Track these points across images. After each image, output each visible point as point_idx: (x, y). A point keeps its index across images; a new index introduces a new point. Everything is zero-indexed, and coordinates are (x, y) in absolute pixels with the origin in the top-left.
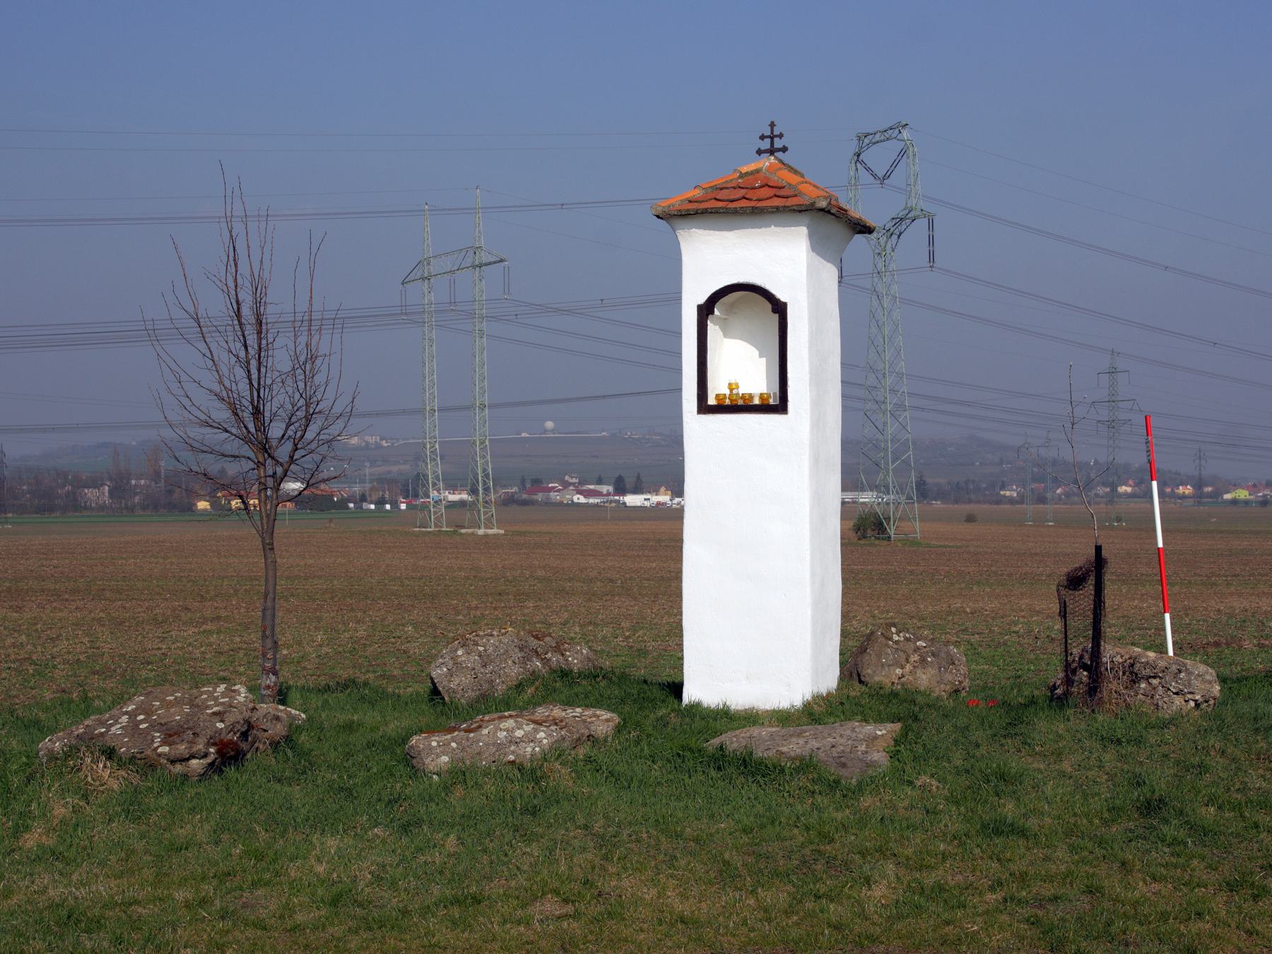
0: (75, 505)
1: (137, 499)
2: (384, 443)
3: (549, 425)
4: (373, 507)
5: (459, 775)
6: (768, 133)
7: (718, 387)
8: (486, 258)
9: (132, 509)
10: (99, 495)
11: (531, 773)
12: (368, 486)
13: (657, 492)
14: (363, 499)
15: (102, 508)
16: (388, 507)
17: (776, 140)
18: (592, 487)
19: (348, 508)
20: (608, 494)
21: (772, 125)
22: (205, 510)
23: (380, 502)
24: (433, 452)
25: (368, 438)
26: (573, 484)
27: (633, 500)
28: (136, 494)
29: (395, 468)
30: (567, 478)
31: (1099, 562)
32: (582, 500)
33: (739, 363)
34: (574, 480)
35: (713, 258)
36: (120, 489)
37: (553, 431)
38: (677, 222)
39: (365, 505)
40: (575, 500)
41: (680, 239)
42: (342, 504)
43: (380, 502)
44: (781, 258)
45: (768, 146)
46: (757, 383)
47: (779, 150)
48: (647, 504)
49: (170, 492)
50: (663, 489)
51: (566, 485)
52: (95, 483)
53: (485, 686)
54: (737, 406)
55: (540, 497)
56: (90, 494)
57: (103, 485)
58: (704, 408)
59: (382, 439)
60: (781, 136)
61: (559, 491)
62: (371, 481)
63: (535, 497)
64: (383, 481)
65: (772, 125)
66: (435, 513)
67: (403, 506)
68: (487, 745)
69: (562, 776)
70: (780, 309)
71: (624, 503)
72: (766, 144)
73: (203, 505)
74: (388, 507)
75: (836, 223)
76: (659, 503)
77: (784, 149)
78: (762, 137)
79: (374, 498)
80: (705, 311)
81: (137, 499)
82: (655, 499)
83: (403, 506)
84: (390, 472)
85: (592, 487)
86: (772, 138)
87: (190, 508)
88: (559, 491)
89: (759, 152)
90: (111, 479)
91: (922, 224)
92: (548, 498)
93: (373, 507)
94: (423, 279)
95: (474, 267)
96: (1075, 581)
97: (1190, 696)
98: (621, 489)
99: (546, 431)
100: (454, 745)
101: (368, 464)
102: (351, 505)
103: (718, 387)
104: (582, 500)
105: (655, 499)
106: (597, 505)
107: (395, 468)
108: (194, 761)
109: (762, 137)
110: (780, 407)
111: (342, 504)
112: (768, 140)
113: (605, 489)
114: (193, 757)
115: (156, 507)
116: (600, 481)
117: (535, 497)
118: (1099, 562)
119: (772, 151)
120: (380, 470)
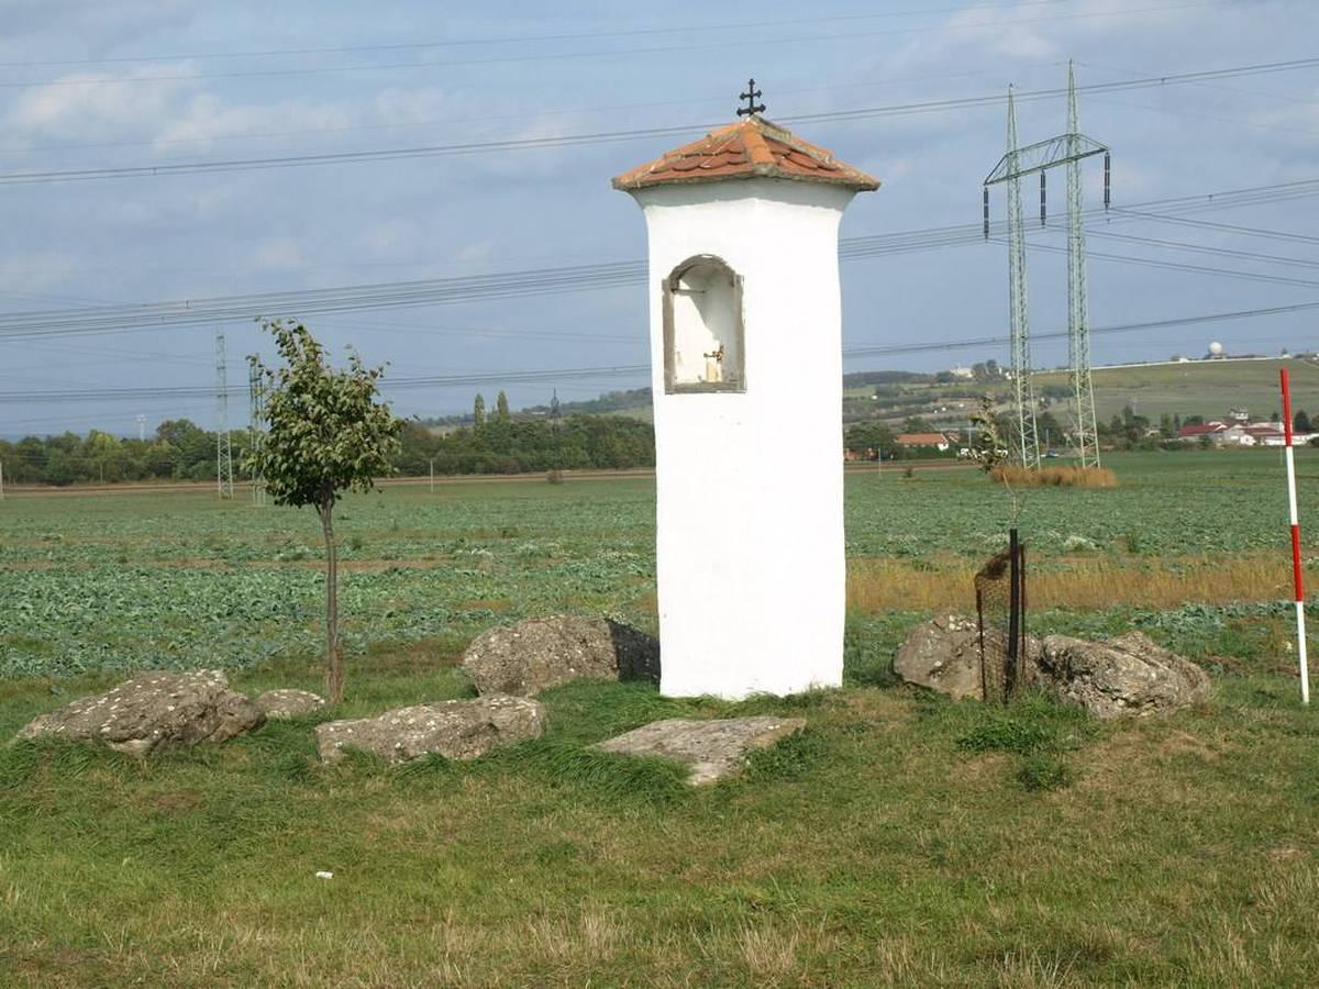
6: (747, 92)
17: (755, 98)
18: (1265, 425)
21: (752, 83)
26: (1241, 422)
31: (1016, 550)
37: (1221, 356)
38: (645, 197)
41: (648, 219)
45: (748, 106)
47: (757, 109)
51: (1231, 422)
53: (513, 674)
58: (673, 389)
60: (759, 94)
65: (752, 83)
66: (1029, 463)
68: (379, 731)
72: (745, 104)
77: (762, 108)
78: (743, 97)
86: (751, 96)
89: (740, 113)
97: (1117, 694)
100: (350, 731)
108: (136, 742)
109: (743, 97)
112: (748, 99)
114: (134, 736)
118: (1016, 550)
119: (751, 111)
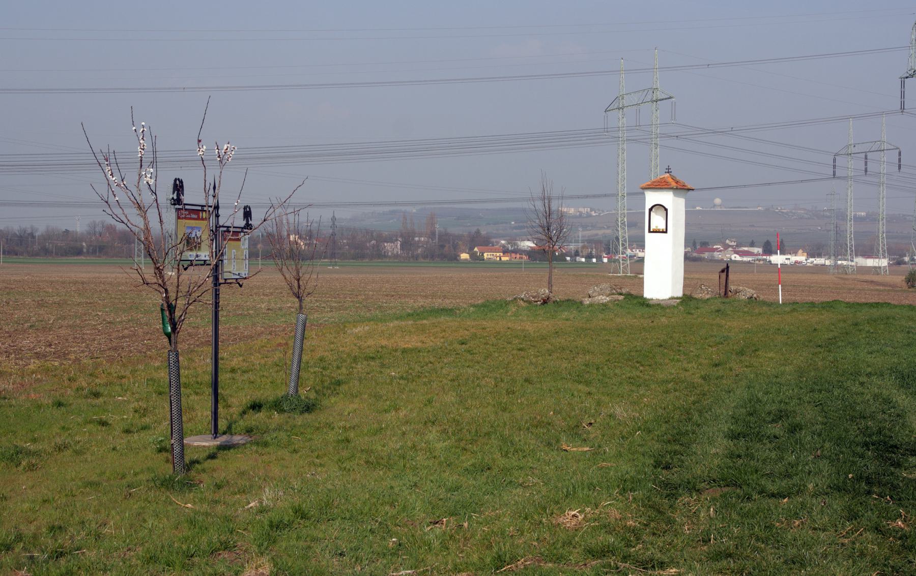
0: (379, 254)
1: (420, 251)
2: (593, 214)
3: (718, 201)
4: (583, 260)
5: (591, 305)
7: (653, 227)
8: (660, 95)
9: (416, 258)
10: (393, 248)
11: (605, 305)
12: (580, 245)
13: (796, 253)
14: (577, 254)
15: (396, 256)
16: (594, 260)
18: (746, 249)
19: (566, 260)
20: (758, 254)
22: (466, 260)
23: (589, 257)
24: (623, 224)
25: (581, 209)
27: (778, 259)
28: (419, 247)
29: (600, 232)
30: (727, 241)
32: (738, 258)
33: (658, 221)
34: (733, 244)
35: (652, 198)
36: (408, 244)
39: (578, 259)
40: (733, 258)
42: (562, 258)
43: (589, 257)
44: (666, 198)
46: (663, 227)
48: (787, 262)
49: (442, 246)
50: (800, 251)
51: (726, 247)
52: (391, 239)
54: (656, 231)
55: (706, 255)
56: (388, 246)
57: (397, 240)
58: (650, 232)
59: (591, 211)
61: (721, 251)
62: (583, 242)
63: (702, 255)
64: (591, 241)
67: (605, 260)
69: (610, 305)
70: (666, 210)
71: (770, 261)
73: (464, 256)
74: (594, 260)
75: (680, 188)
76: (796, 262)
79: (585, 253)
80: (651, 210)
81: (420, 251)
82: (794, 259)
83: (605, 260)
84: (597, 235)
85: (746, 249)
87: (455, 258)
88: (721, 251)
90: (401, 236)
92: (713, 257)
93: (583, 260)
94: (619, 109)
95: (652, 101)
96: (723, 271)
98: (768, 251)
99: (715, 206)
101: (580, 229)
102: (568, 258)
103: (653, 227)
104: (738, 258)
105: (794, 259)
106: (749, 262)
107: (600, 232)
110: (666, 232)
111: (562, 258)
113: (756, 250)
115: (432, 257)
116: (752, 245)
117: (702, 255)
120: (588, 233)
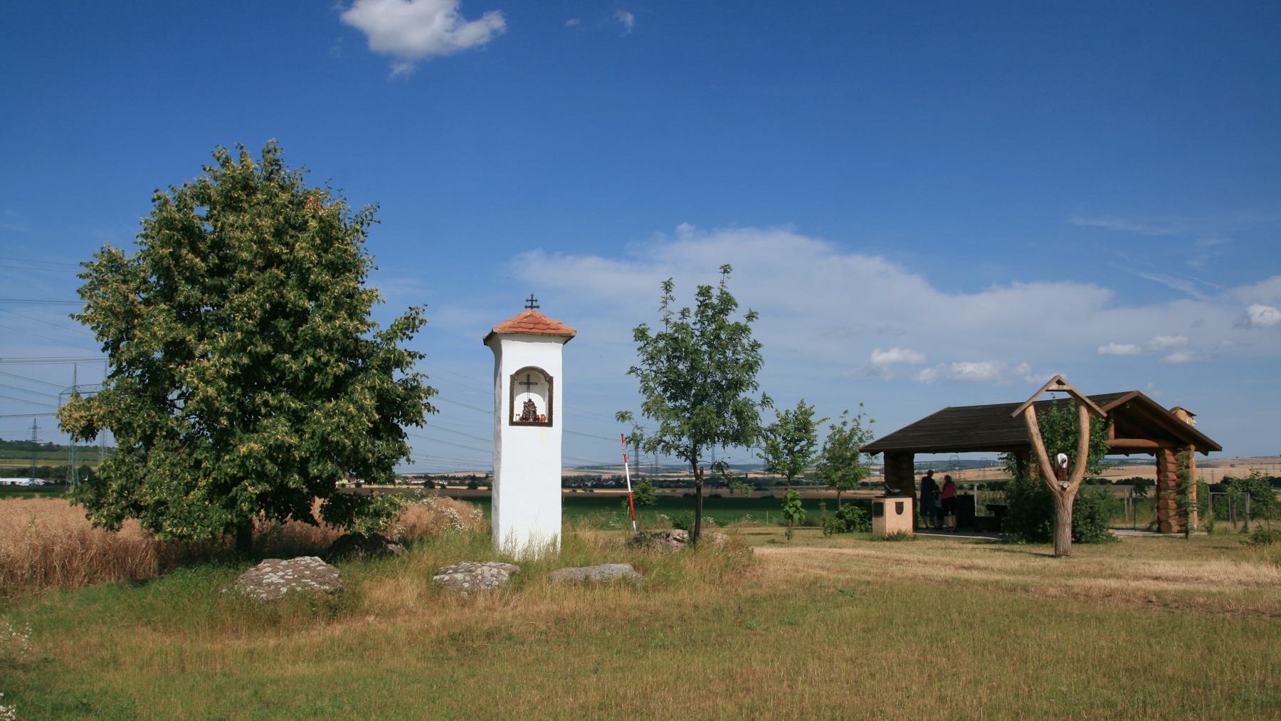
58: (512, 423)
72: (529, 304)
80: (513, 378)
91: (516, 419)
110: (550, 424)
119: (532, 307)
